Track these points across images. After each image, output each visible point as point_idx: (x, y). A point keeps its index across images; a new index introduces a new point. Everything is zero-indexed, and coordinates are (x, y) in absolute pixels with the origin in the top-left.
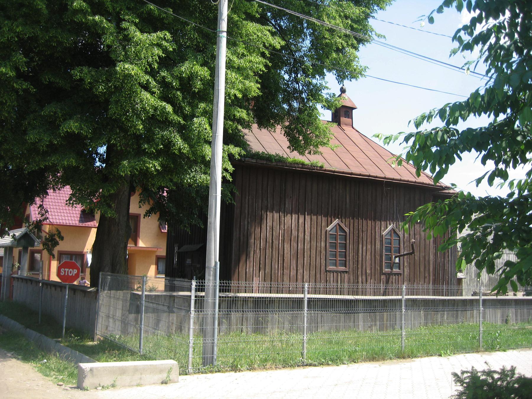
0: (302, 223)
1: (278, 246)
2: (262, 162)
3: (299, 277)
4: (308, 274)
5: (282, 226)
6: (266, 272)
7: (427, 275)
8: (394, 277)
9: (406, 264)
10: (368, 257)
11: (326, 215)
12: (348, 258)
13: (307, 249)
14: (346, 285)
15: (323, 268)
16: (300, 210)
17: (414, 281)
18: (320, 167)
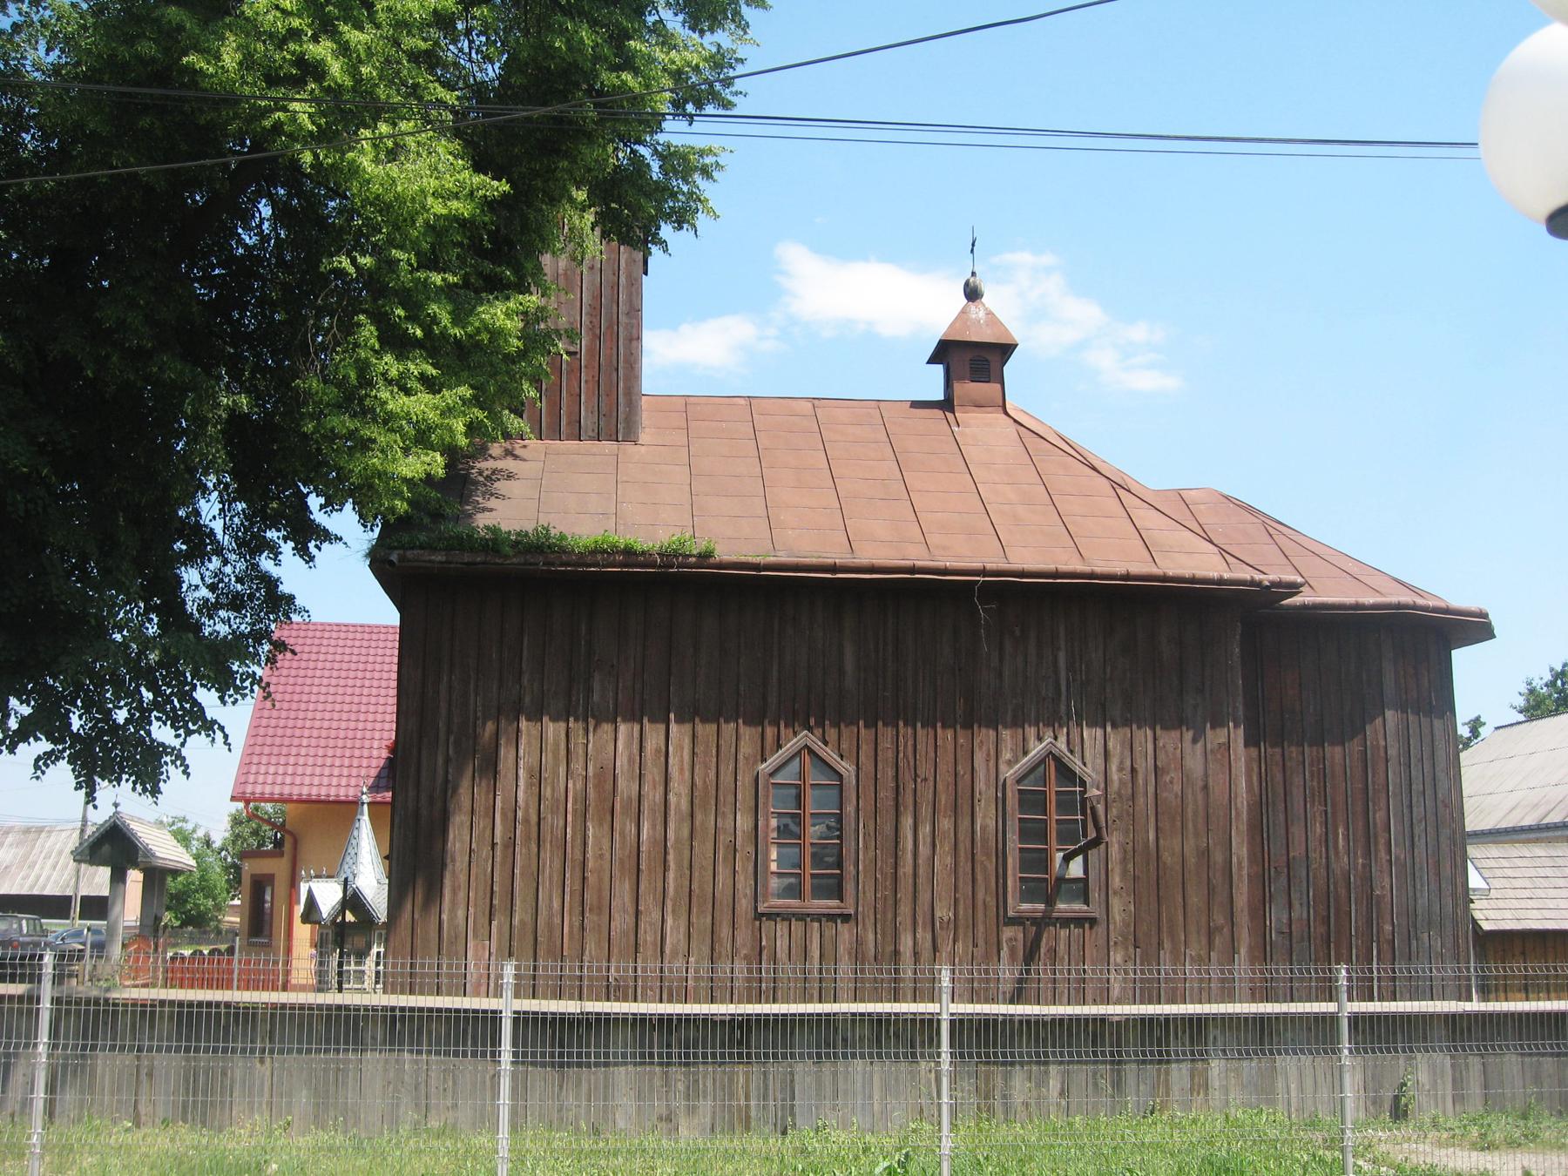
0: (658, 751)
1: (560, 833)
2: (467, 558)
3: (648, 936)
4: (683, 929)
5: (577, 766)
6: (516, 921)
7: (1219, 919)
8: (1064, 933)
9: (1116, 881)
10: (944, 859)
11: (756, 718)
12: (849, 868)
13: (677, 840)
14: (845, 968)
15: (744, 904)
16: (646, 705)
17: (1160, 945)
18: (700, 556)
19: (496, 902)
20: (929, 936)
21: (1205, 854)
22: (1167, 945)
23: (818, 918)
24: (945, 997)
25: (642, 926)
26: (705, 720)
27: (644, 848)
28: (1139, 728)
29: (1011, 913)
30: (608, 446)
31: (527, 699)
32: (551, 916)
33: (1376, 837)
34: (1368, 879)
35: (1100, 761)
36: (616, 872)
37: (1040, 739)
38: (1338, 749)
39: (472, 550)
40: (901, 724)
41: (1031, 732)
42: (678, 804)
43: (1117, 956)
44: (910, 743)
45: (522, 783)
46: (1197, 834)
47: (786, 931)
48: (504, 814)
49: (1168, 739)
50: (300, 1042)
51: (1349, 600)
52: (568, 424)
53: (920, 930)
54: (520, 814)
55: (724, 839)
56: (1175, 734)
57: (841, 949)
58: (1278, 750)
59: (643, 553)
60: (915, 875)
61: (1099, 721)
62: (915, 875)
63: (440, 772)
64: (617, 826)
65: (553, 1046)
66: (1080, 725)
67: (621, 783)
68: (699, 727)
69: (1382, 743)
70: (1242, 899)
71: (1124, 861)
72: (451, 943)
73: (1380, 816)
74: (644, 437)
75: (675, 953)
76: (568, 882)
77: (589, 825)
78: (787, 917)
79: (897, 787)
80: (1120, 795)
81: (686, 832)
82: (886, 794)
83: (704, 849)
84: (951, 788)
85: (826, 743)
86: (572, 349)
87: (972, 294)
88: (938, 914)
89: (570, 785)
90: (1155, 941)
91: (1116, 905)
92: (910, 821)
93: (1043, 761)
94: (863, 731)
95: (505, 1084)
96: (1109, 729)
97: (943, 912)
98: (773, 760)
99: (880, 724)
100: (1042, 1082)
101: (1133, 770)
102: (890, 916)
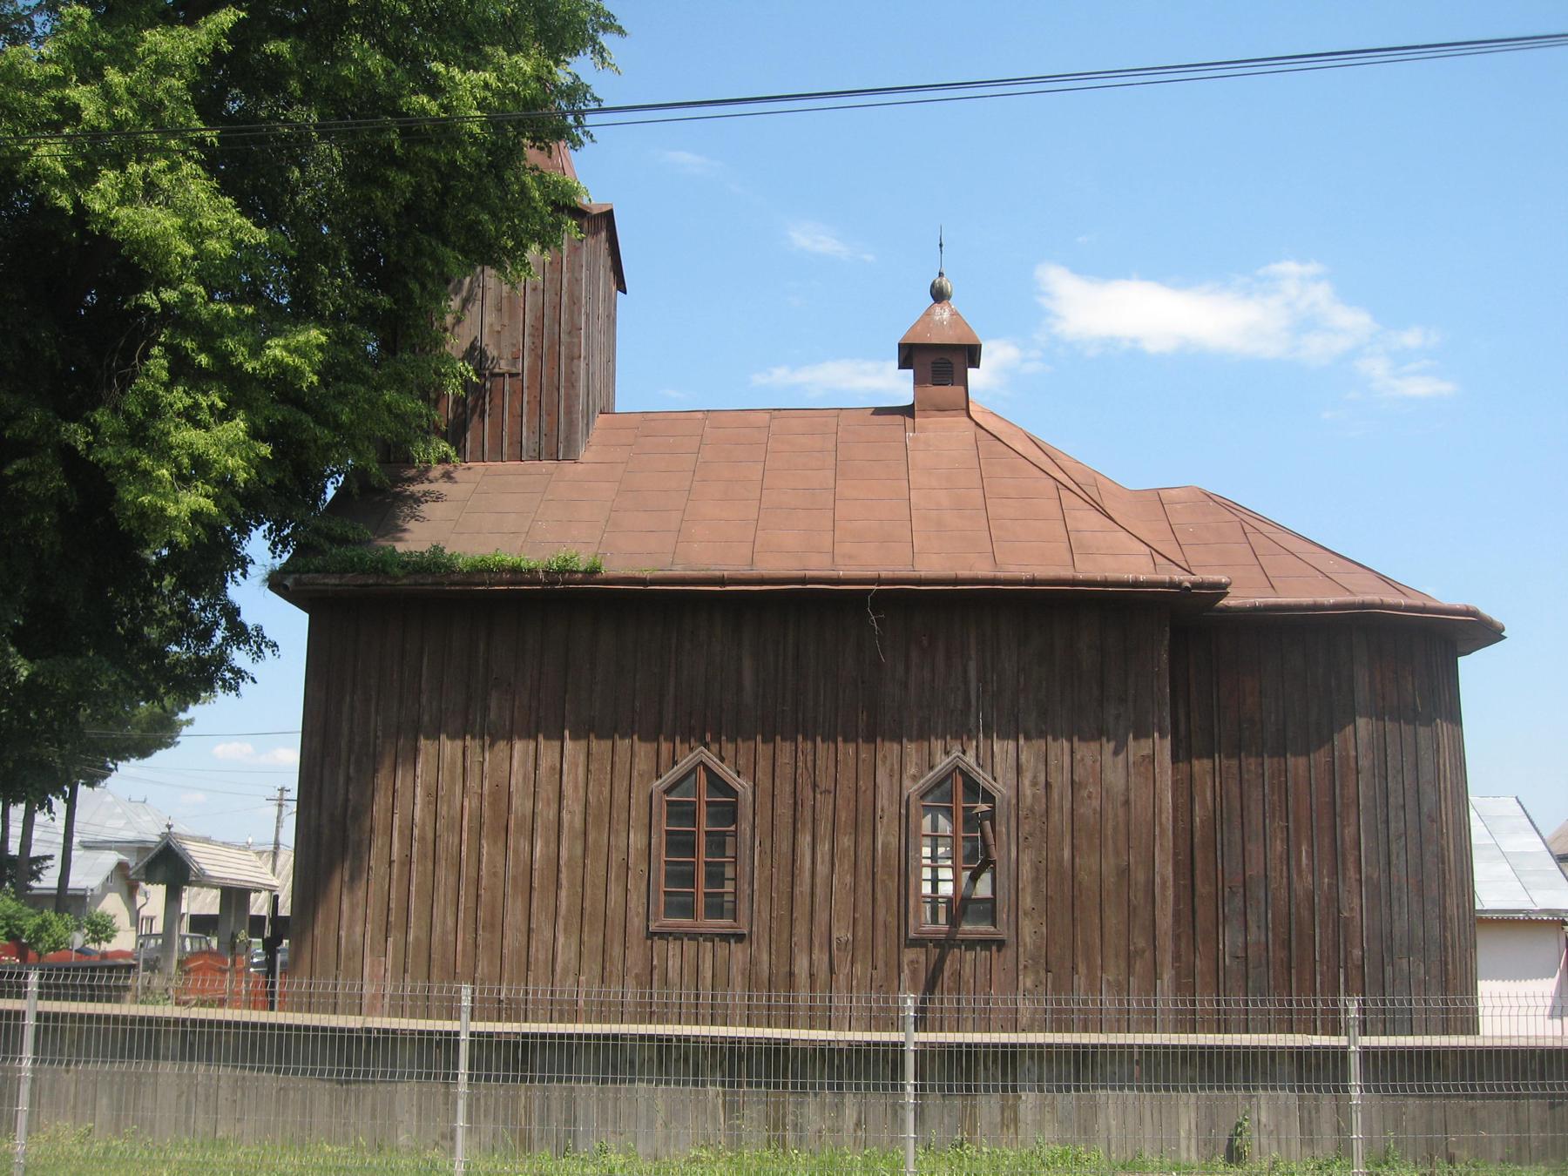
0: (553, 768)
3: (539, 953)
5: (473, 783)
6: (411, 938)
7: (1141, 942)
8: (969, 956)
9: (1027, 901)
10: (842, 878)
11: (651, 735)
13: (570, 859)
15: (636, 923)
16: (542, 723)
17: (1074, 969)
18: (585, 572)
19: (392, 919)
20: (826, 958)
21: (1125, 873)
22: (1082, 969)
23: (711, 937)
24: (465, 1016)
25: (533, 944)
26: (599, 737)
27: (536, 866)
28: (1055, 739)
29: (912, 935)
30: (547, 465)
31: (426, 718)
32: (444, 933)
33: (1344, 855)
34: (1334, 900)
35: (1012, 775)
36: (509, 889)
37: (947, 753)
38: (1302, 761)
39: (363, 572)
40: (800, 738)
41: (938, 745)
42: (571, 822)
43: (1027, 981)
44: (810, 758)
45: (418, 800)
46: (1117, 853)
47: (678, 951)
48: (401, 832)
49: (1086, 751)
50: (253, 1061)
51: (1306, 600)
52: (510, 444)
53: (816, 951)
54: (416, 832)
55: (616, 857)
56: (1094, 746)
57: (734, 970)
58: (1235, 762)
59: (530, 571)
60: (812, 894)
61: (1012, 731)
62: (812, 894)
63: (341, 791)
64: (511, 843)
65: (332, 1064)
66: (988, 736)
67: (516, 801)
68: (594, 744)
69: (1353, 753)
70: (1165, 922)
71: (1036, 880)
72: (348, 958)
73: (1349, 832)
74: (585, 454)
75: (566, 971)
76: (462, 900)
77: (484, 842)
78: (678, 937)
79: (795, 803)
80: (1032, 810)
81: (579, 851)
82: (784, 811)
83: (596, 868)
84: (852, 804)
85: (722, 760)
86: (514, 371)
87: (939, 295)
88: (835, 935)
89: (466, 803)
90: (1068, 965)
91: (1027, 927)
92: (808, 838)
93: (949, 776)
94: (760, 746)
95: (462, 1106)
96: (1022, 741)
97: (841, 933)
98: (669, 777)
99: (778, 738)
100: (839, 1107)
101: (1048, 785)
102: (785, 936)
